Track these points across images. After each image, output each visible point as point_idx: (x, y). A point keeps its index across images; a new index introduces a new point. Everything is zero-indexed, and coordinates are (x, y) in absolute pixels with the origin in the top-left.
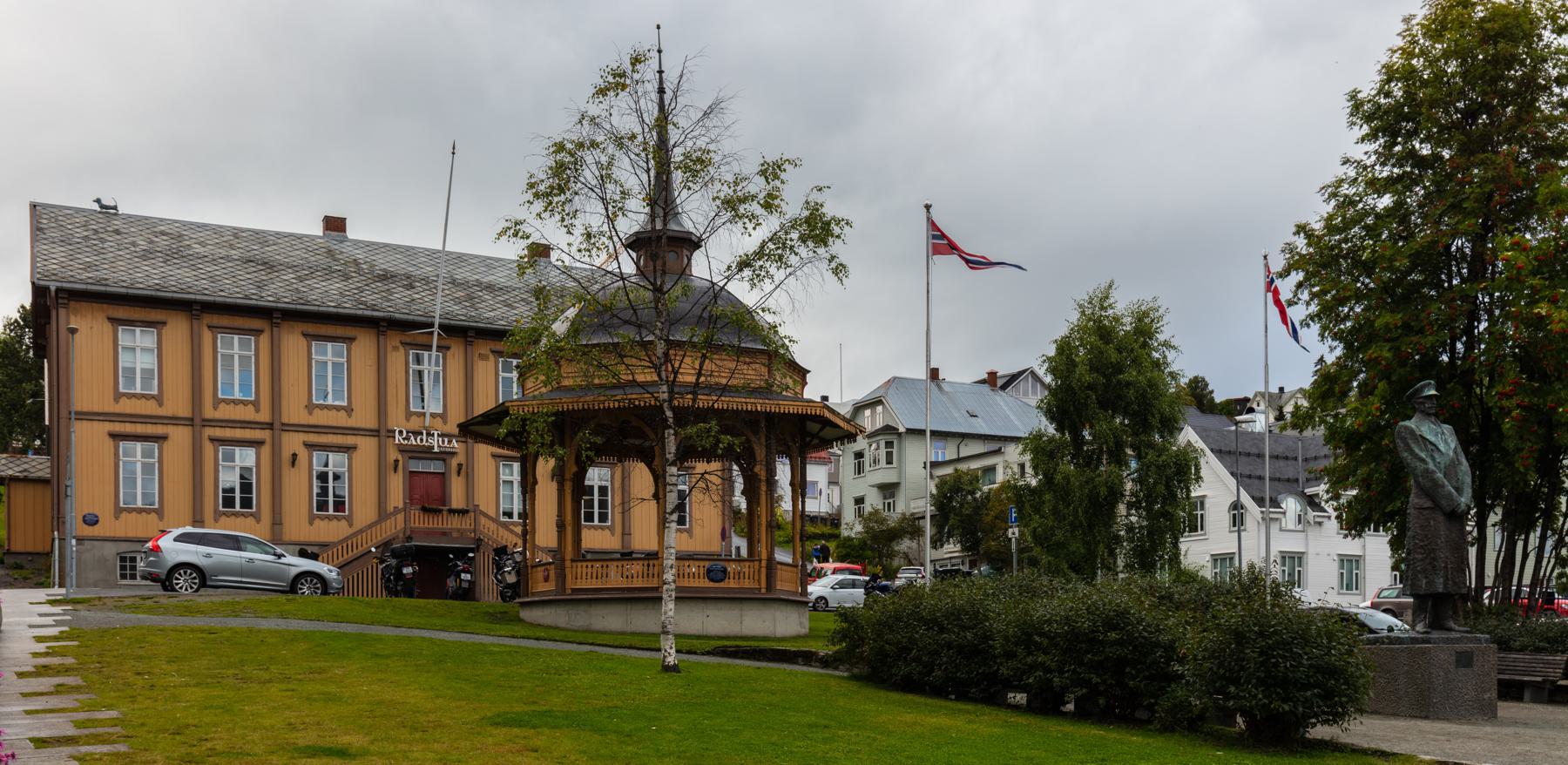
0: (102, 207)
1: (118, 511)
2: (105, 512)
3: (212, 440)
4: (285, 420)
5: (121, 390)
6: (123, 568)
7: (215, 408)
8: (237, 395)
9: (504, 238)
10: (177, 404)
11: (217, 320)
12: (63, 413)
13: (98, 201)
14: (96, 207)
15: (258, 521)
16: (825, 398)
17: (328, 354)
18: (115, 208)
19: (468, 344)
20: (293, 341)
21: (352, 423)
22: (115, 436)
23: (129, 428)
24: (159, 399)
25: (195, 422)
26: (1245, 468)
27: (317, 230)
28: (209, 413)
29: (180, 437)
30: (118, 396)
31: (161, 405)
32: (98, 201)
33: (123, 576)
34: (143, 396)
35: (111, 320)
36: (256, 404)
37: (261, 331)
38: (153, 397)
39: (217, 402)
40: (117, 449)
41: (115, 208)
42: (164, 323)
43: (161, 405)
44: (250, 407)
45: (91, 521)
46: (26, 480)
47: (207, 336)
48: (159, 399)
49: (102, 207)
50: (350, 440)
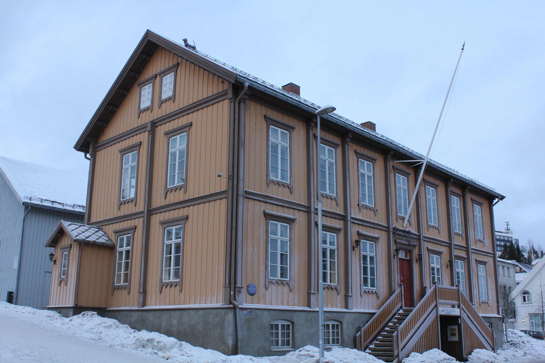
37: (338, 145)
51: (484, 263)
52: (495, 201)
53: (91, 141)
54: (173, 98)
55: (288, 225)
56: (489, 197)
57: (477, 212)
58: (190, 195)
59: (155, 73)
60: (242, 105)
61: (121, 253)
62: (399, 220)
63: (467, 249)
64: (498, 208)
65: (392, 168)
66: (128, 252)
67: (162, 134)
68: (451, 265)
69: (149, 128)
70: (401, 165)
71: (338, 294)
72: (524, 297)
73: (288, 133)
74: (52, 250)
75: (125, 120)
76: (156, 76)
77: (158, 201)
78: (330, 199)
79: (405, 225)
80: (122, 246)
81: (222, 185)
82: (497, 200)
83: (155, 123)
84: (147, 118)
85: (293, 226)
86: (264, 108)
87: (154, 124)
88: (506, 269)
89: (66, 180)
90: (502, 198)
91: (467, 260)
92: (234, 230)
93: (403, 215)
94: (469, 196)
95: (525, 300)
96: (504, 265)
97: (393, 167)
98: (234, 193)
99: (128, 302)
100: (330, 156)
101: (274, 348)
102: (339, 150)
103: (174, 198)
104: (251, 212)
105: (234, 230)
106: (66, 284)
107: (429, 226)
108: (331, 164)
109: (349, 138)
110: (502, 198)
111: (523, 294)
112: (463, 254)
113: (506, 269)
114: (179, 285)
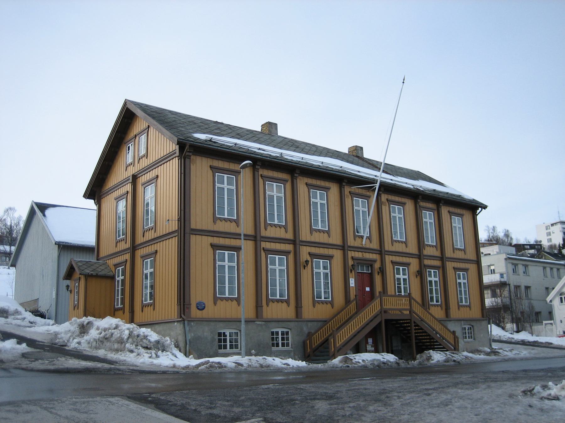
1: (216, 300)
2: (208, 302)
4: (193, 226)
6: (220, 341)
8: (276, 222)
10: (246, 227)
12: (187, 230)
15: (288, 305)
16: (541, 241)
20: (302, 183)
22: (215, 247)
25: (295, 242)
26: (255, 139)
28: (263, 233)
29: (247, 247)
30: (215, 219)
33: (220, 347)
36: (285, 227)
37: (286, 181)
38: (234, 221)
42: (405, 204)
44: (326, 234)
45: (201, 307)
46: (97, 276)
51: (466, 270)
52: (478, 211)
53: (96, 190)
54: (146, 155)
55: (236, 253)
56: (472, 208)
57: (457, 223)
58: (158, 234)
59: (135, 134)
60: (187, 160)
61: (118, 281)
62: (357, 238)
63: (442, 258)
64: (482, 217)
65: (349, 194)
66: (122, 280)
67: (140, 186)
68: (420, 274)
69: (131, 181)
70: (364, 190)
71: (288, 305)
72: (561, 298)
73: (234, 177)
74: (68, 282)
75: (121, 173)
76: (136, 136)
77: (140, 239)
78: (278, 228)
79: (364, 243)
80: (118, 276)
81: (174, 226)
82: (480, 209)
83: (136, 176)
84: (132, 171)
85: (240, 253)
86: (209, 160)
87: (135, 178)
88: (555, 270)
89: (77, 223)
90: (485, 207)
91: (443, 268)
92: (182, 261)
93: (362, 234)
94: (445, 210)
95: (562, 302)
96: (552, 266)
97: (350, 192)
98: (185, 231)
99: (502, 324)
100: (279, 191)
101: (222, 351)
102: (289, 185)
103: (150, 235)
104: (199, 246)
105: (182, 261)
106: (78, 308)
107: (393, 241)
108: (279, 198)
109: (297, 173)
110: (485, 207)
111: (561, 295)
112: (437, 263)
113: (555, 270)
114: (153, 305)
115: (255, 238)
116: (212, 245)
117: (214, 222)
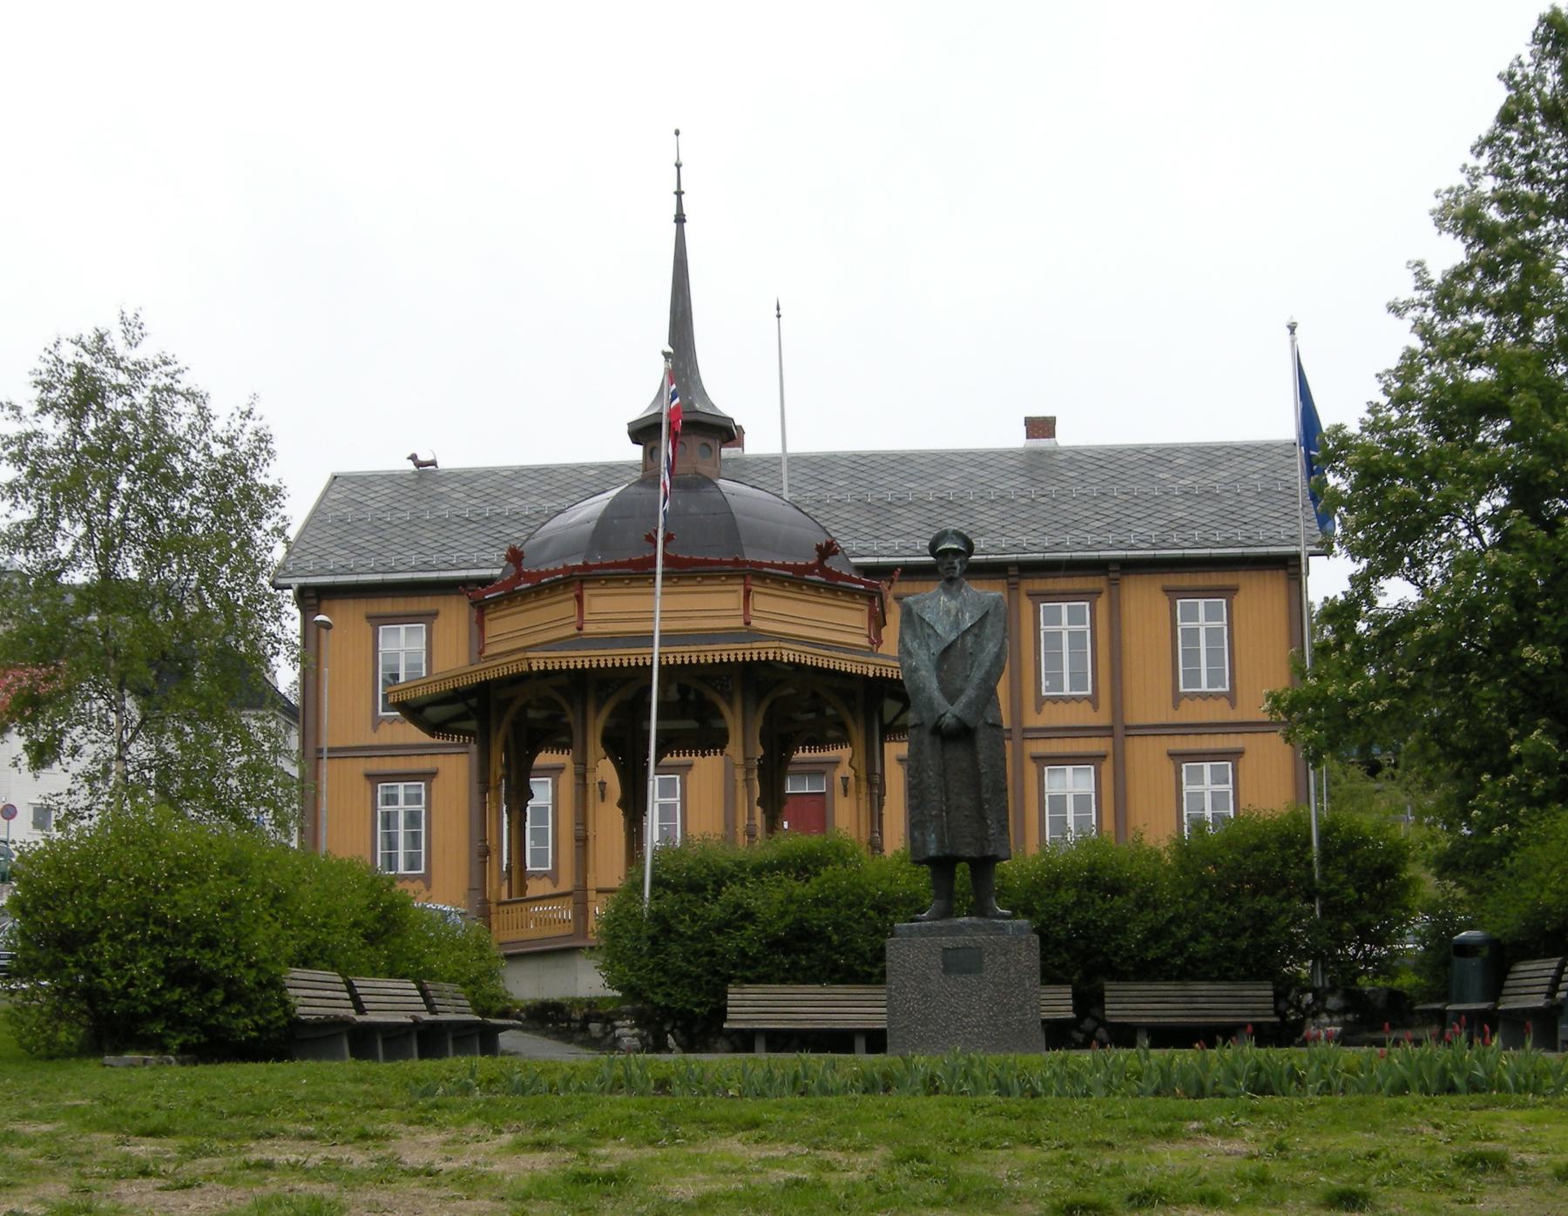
0: (419, 464)
3: (1035, 758)
4: (1129, 722)
5: (1044, 693)
7: (1038, 710)
9: (181, 366)
11: (1039, 585)
13: (413, 457)
14: (411, 466)
17: (1202, 619)
18: (433, 463)
19: (1114, 583)
20: (1142, 597)
21: (1233, 716)
22: (374, 778)
23: (388, 765)
24: (1231, 697)
25: (1119, 731)
27: (1017, 439)
31: (1233, 705)
32: (413, 457)
34: (1074, 698)
35: (1167, 591)
36: (1093, 700)
39: (1041, 702)
40: (1178, 773)
41: (433, 463)
42: (435, 614)
43: (1233, 705)
47: (1027, 605)
48: (1231, 697)
49: (419, 464)
50: (822, 768)
102: (1102, 603)
115: (1119, 731)
116: (1173, 755)
117: (1176, 706)
